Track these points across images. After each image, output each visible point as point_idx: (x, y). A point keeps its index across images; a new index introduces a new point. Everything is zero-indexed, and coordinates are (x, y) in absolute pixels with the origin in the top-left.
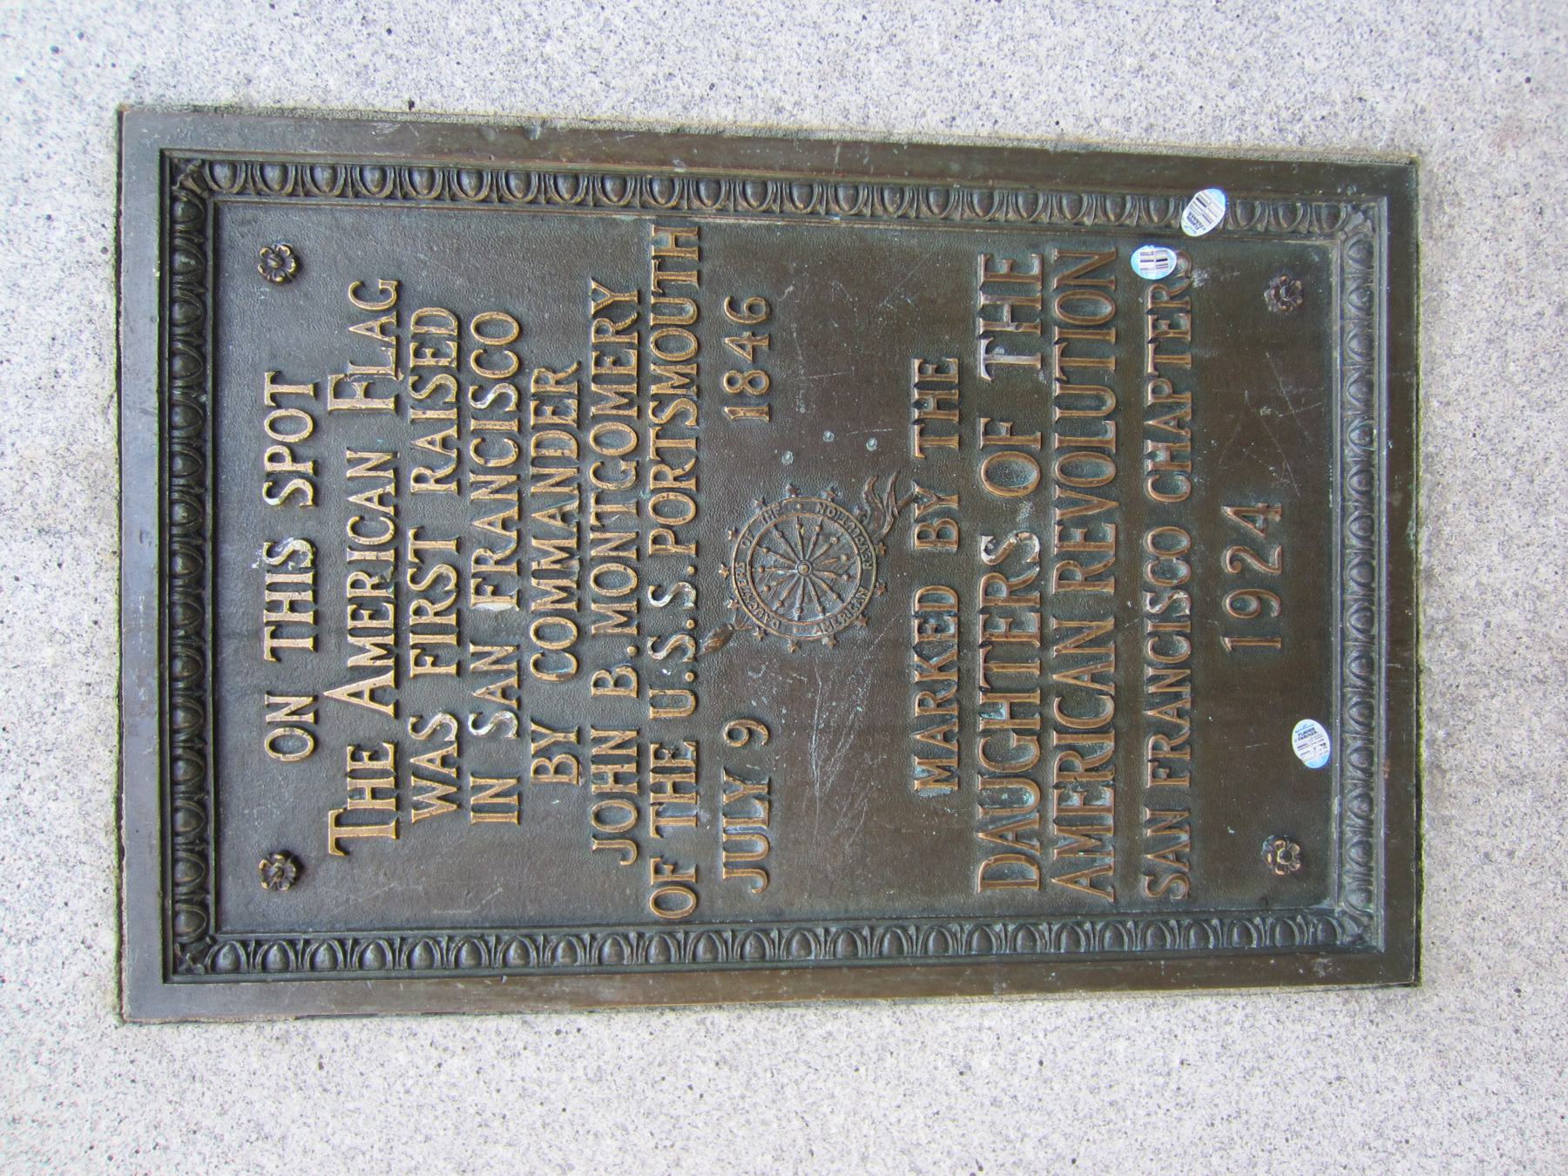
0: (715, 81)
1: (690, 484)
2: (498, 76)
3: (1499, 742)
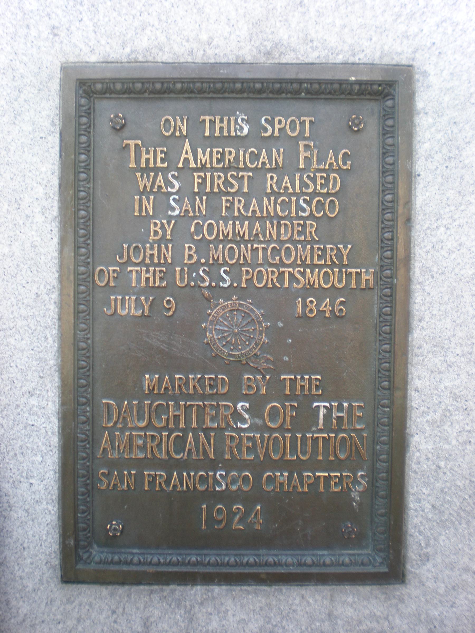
0: (431, 295)
1: (270, 285)
2: (431, 209)
3: (162, 618)
